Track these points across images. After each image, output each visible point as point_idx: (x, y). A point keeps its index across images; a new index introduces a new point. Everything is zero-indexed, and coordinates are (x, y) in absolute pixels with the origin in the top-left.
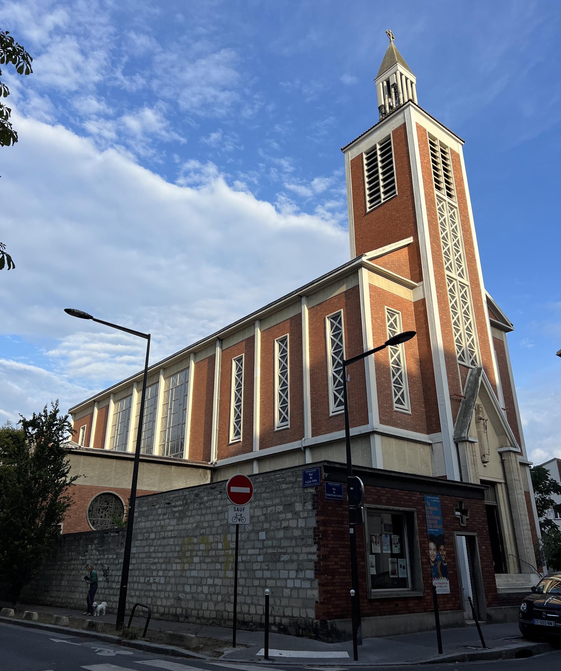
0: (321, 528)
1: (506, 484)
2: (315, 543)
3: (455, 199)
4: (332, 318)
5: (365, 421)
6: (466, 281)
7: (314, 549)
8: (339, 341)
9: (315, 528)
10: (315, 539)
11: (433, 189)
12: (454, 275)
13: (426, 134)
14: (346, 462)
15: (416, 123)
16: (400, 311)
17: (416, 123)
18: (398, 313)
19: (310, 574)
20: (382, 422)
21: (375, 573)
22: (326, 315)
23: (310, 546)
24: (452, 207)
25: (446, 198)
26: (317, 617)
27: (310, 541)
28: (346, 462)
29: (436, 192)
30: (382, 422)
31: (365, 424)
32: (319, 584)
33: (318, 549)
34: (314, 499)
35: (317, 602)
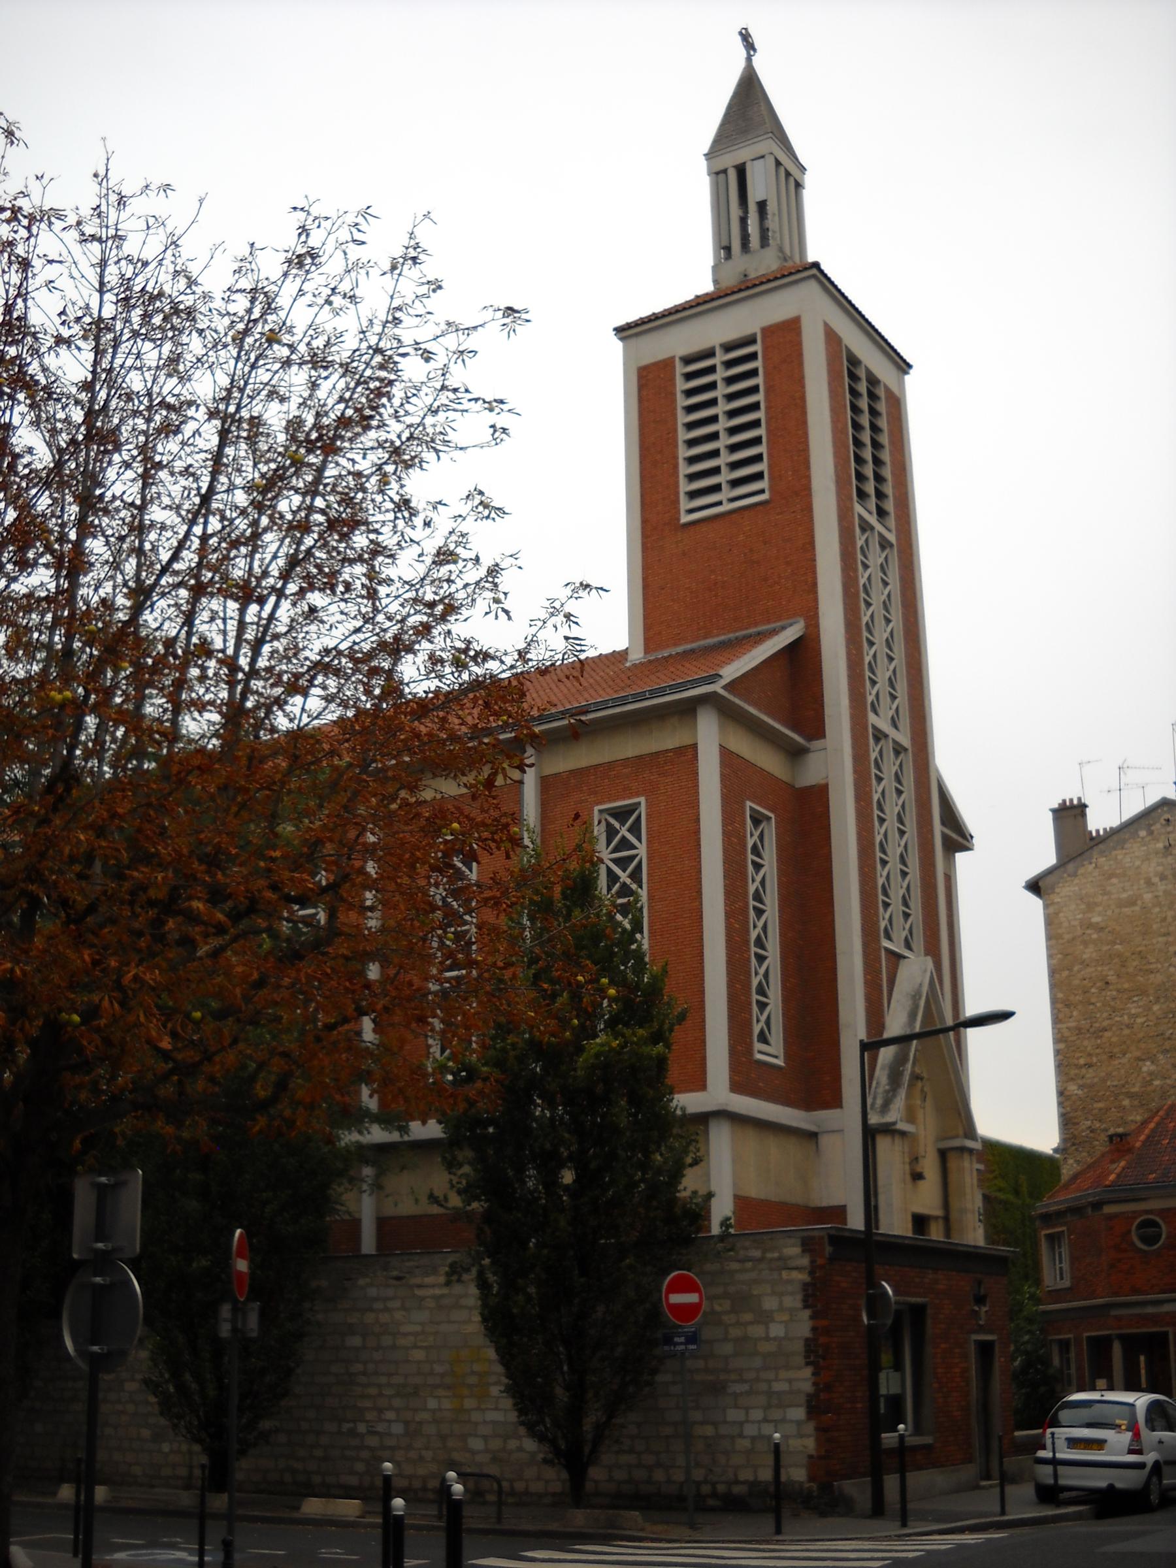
0: (822, 1340)
1: (946, 1219)
2: (807, 1364)
3: (892, 521)
4: (610, 815)
5: (700, 1084)
6: (905, 740)
7: (808, 1372)
8: (631, 876)
9: (807, 1340)
10: (806, 1357)
11: (851, 499)
12: (885, 726)
13: (841, 351)
14: (863, 1228)
15: (826, 325)
16: (772, 811)
17: (826, 325)
18: (769, 819)
19: (799, 1413)
20: (737, 1087)
21: (97, 1488)
22: (597, 804)
23: (799, 1368)
24: (884, 544)
25: (873, 520)
26: (812, 1478)
27: (800, 1360)
28: (863, 1228)
29: (858, 508)
30: (737, 1087)
31: (697, 1090)
32: (817, 1429)
33: (813, 1374)
34: (805, 1290)
35: (811, 1457)
